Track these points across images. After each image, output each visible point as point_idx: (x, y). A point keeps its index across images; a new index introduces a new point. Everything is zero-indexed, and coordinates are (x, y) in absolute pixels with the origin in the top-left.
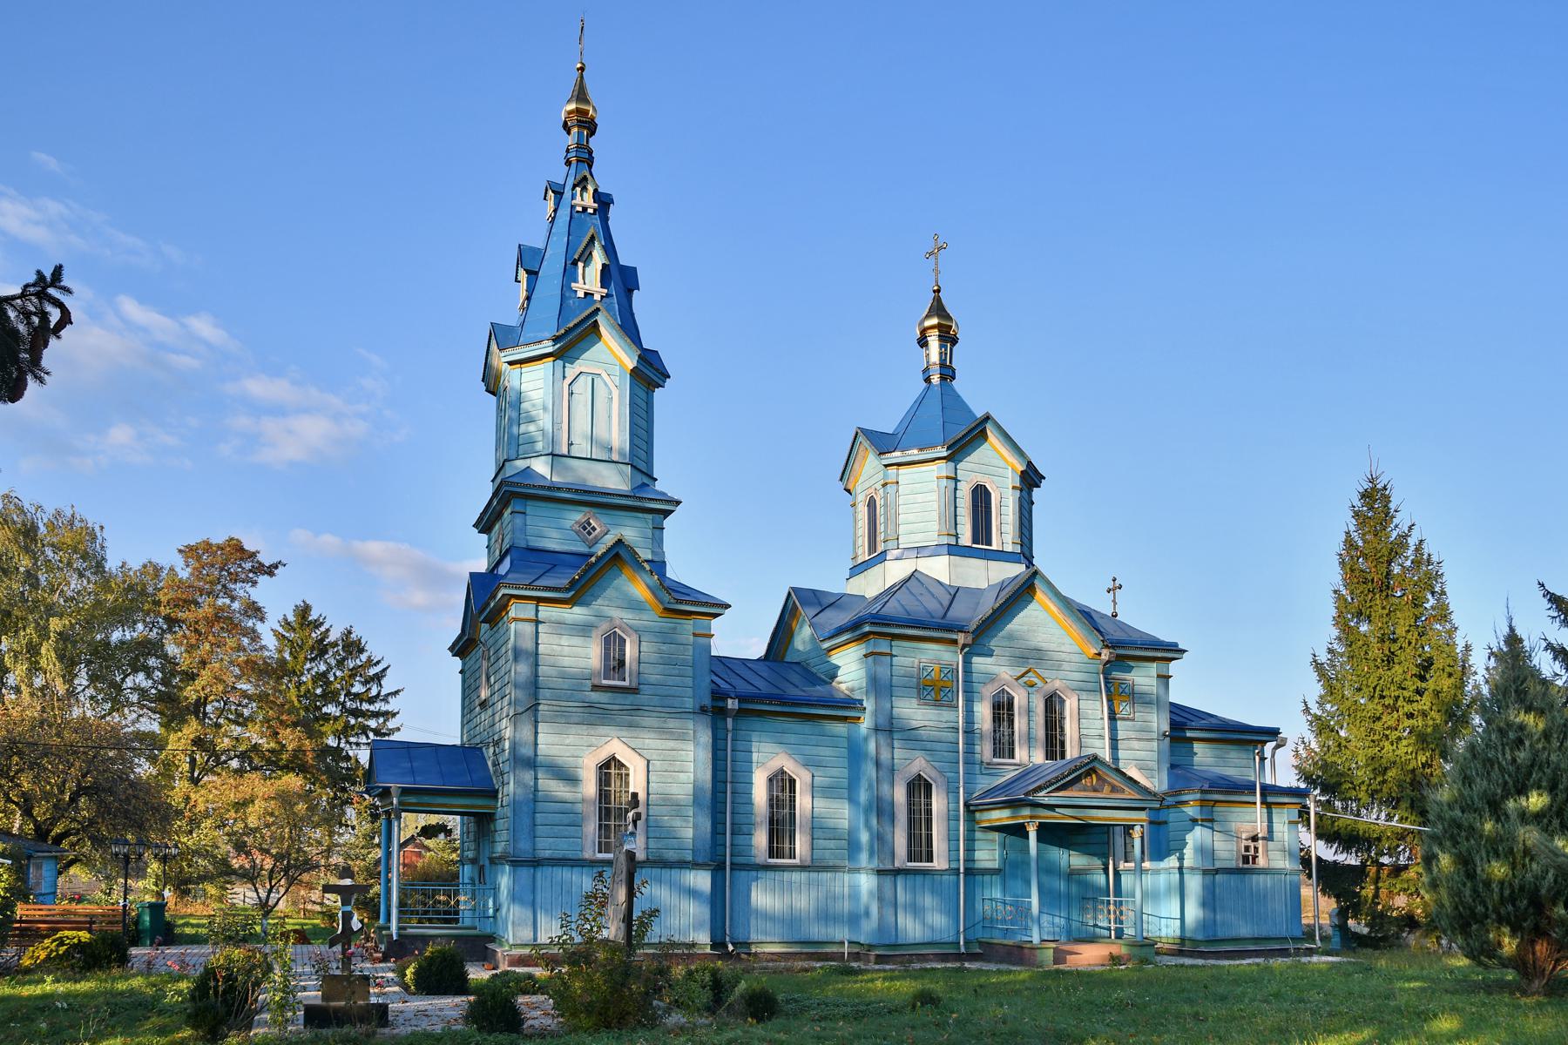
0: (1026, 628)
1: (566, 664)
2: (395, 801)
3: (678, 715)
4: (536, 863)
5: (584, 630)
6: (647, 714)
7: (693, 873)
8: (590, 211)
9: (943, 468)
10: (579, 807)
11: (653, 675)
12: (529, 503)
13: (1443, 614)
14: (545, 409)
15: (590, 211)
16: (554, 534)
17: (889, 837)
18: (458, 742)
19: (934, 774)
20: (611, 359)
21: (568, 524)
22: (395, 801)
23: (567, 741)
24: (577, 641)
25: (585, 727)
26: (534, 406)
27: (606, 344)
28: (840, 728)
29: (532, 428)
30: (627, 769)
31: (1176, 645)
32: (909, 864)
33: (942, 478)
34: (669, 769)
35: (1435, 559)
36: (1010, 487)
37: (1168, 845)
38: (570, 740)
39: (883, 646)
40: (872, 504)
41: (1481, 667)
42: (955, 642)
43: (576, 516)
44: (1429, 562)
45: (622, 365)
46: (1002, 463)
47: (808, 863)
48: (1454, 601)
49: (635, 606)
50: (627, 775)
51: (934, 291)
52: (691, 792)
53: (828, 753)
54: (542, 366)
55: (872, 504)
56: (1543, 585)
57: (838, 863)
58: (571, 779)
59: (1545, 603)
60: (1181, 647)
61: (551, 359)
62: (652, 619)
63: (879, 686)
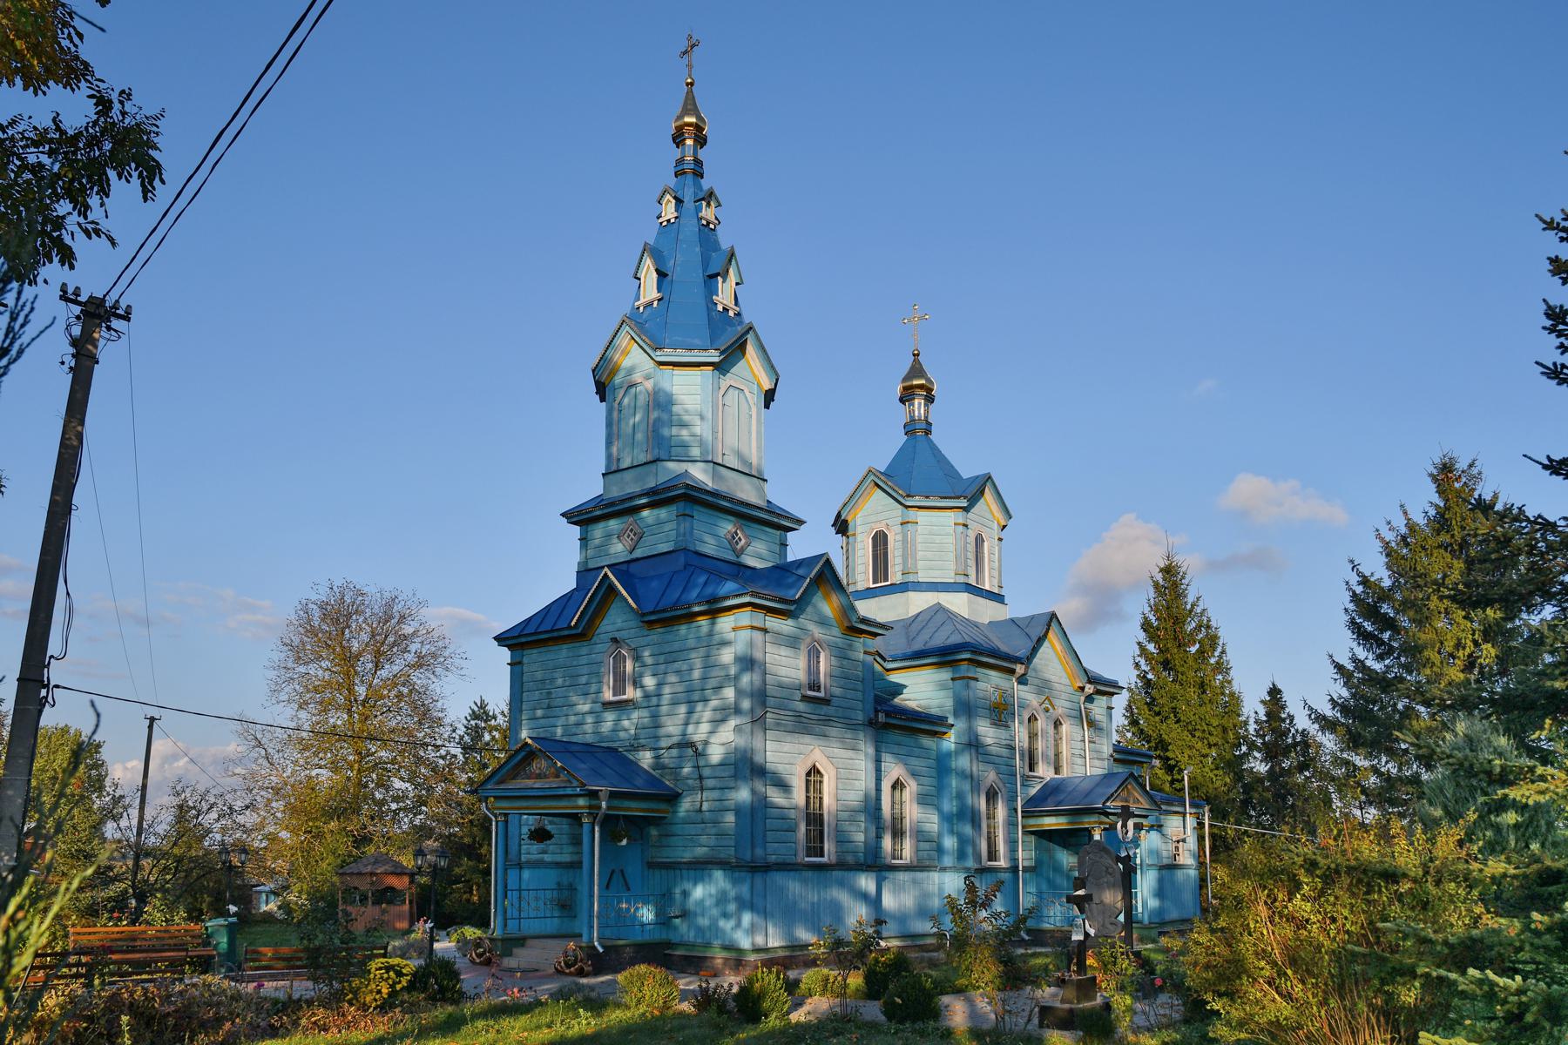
0: (1043, 662)
1: (783, 673)
2: (604, 805)
3: (853, 727)
4: (767, 868)
5: (792, 642)
6: (835, 724)
7: (901, 873)
8: (673, 221)
9: (959, 516)
10: (792, 814)
11: (837, 691)
12: (696, 507)
13: (1221, 667)
14: (702, 418)
15: (673, 221)
16: (708, 538)
17: (978, 842)
18: (42, 724)
19: (1001, 785)
20: (750, 377)
21: (722, 532)
22: (604, 805)
23: (785, 749)
24: (784, 651)
25: (796, 735)
26: (686, 411)
27: (748, 362)
28: (927, 742)
29: (684, 432)
30: (822, 776)
31: (1117, 682)
32: (807, 859)
33: (959, 524)
34: (850, 777)
35: (1213, 623)
36: (996, 538)
37: (765, 836)
38: (787, 747)
39: (964, 669)
40: (880, 541)
41: (1253, 708)
42: (1012, 672)
43: (727, 526)
44: (1208, 627)
45: (759, 385)
46: (990, 517)
47: (915, 864)
48: (1232, 657)
49: (823, 622)
50: (821, 782)
51: (914, 355)
52: (862, 798)
53: (917, 763)
54: (699, 373)
55: (880, 541)
56: (1331, 656)
57: (932, 863)
58: (784, 786)
59: (1332, 670)
60: (1120, 684)
61: (711, 368)
62: (834, 635)
63: (965, 708)
